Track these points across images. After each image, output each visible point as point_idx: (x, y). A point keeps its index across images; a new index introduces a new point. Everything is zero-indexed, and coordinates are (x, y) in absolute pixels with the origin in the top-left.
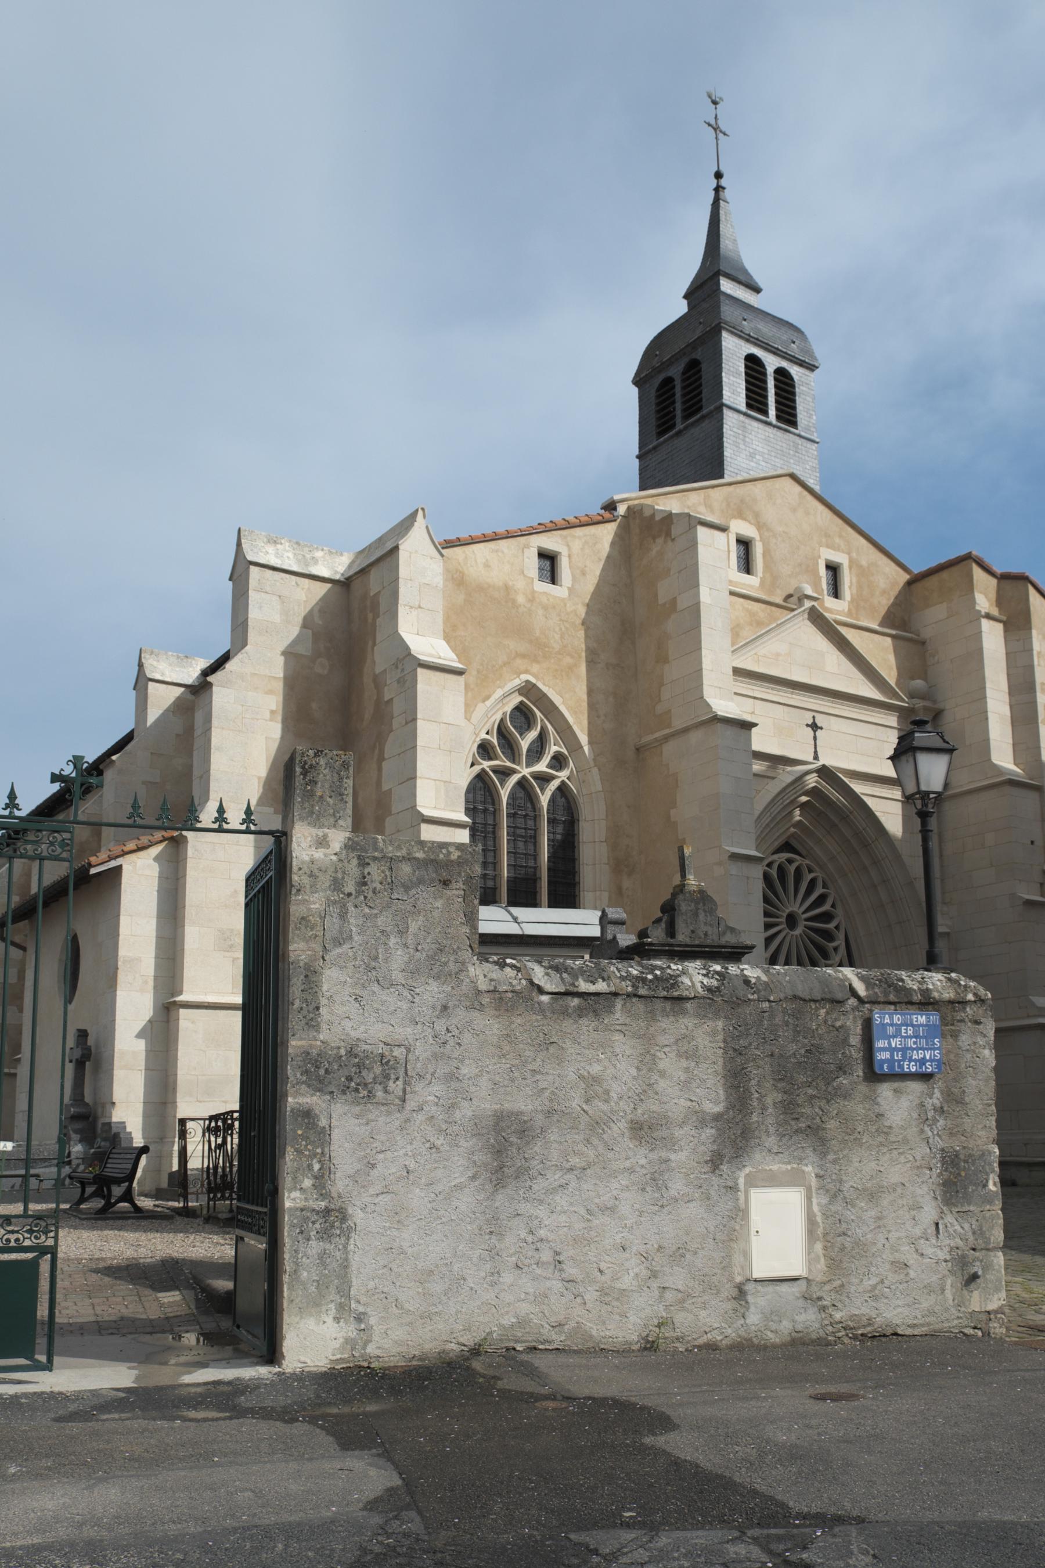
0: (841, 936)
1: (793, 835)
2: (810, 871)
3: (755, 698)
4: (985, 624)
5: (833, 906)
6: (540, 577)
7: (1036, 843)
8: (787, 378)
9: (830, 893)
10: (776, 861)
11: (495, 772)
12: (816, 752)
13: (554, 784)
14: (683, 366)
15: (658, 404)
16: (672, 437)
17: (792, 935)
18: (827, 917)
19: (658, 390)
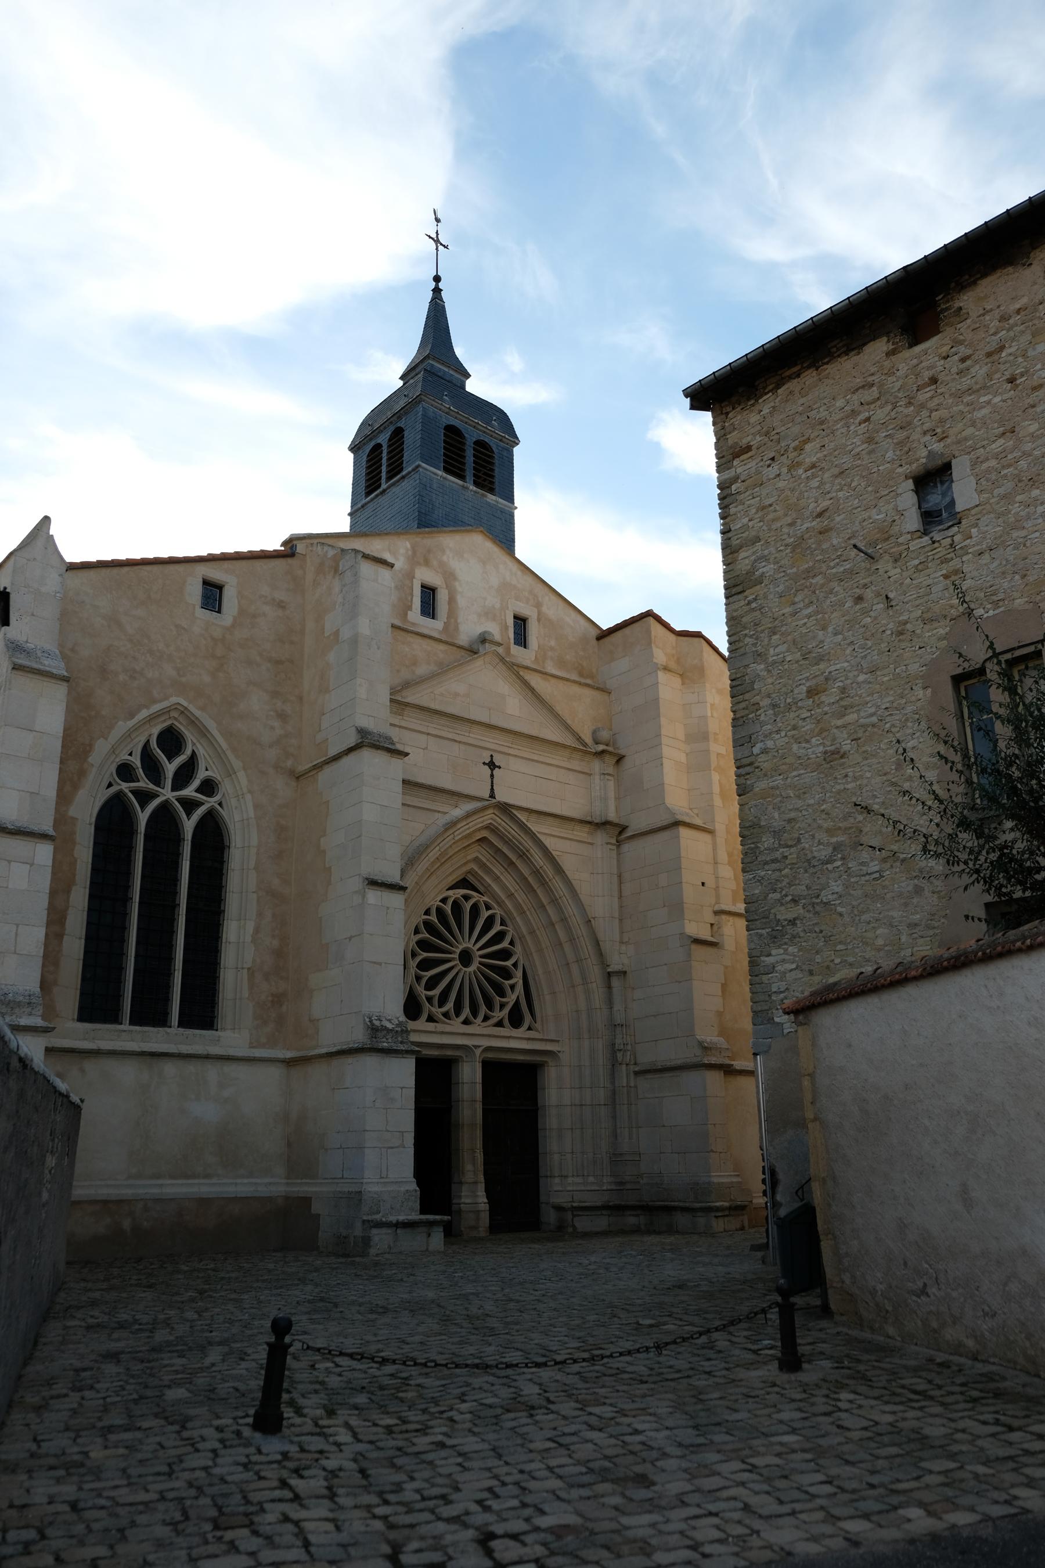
0: (519, 974)
1: (470, 872)
2: (488, 908)
3: (428, 734)
4: (662, 676)
5: (512, 943)
6: (203, 603)
7: (706, 885)
8: (488, 450)
9: (509, 931)
10: (450, 897)
11: (132, 792)
12: (492, 789)
13: (200, 811)
14: (390, 433)
15: (368, 468)
16: (377, 496)
17: (465, 972)
18: (505, 955)
19: (368, 456)
